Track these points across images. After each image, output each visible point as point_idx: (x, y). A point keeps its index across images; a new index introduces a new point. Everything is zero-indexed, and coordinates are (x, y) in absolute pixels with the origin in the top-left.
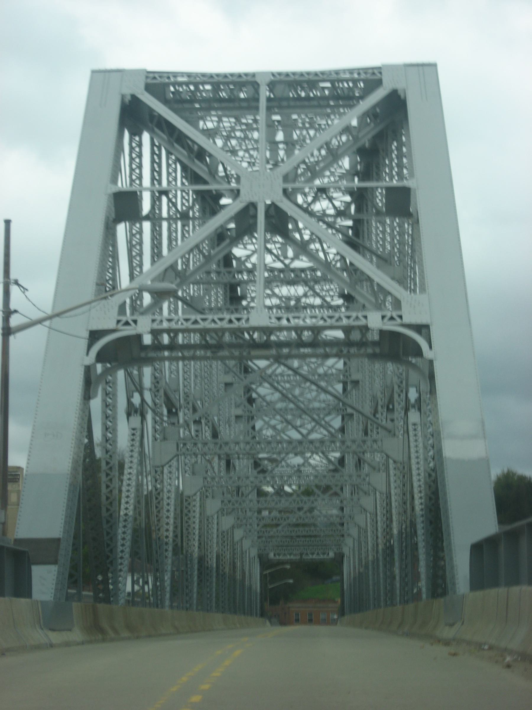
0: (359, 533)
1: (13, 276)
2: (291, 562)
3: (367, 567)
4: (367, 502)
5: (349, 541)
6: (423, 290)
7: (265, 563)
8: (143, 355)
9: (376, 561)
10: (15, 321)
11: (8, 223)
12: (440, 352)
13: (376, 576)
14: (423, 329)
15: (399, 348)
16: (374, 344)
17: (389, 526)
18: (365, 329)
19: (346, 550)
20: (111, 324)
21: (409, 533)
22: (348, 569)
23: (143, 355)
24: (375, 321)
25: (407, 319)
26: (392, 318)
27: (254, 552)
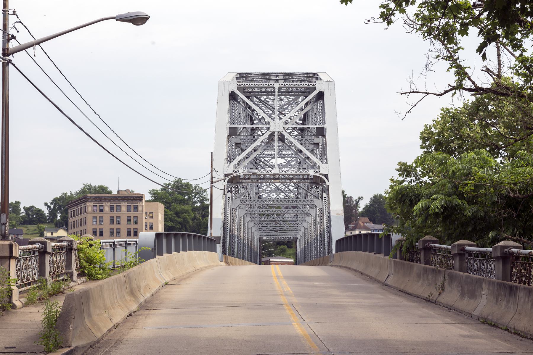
0: (305, 230)
1: (213, 167)
2: (273, 241)
3: (308, 245)
4: (308, 219)
5: (300, 233)
6: (327, 163)
7: (261, 241)
8: (240, 181)
9: (311, 242)
10: (214, 180)
11: (212, 153)
12: (331, 183)
13: (493, 76)
14: (326, 176)
15: (319, 182)
16: (311, 179)
17: (316, 229)
18: (309, 175)
19: (299, 237)
20: (231, 172)
21: (322, 234)
22: (300, 246)
23: (240, 181)
24: (312, 173)
25: (321, 173)
26: (317, 172)
27: (258, 237)
